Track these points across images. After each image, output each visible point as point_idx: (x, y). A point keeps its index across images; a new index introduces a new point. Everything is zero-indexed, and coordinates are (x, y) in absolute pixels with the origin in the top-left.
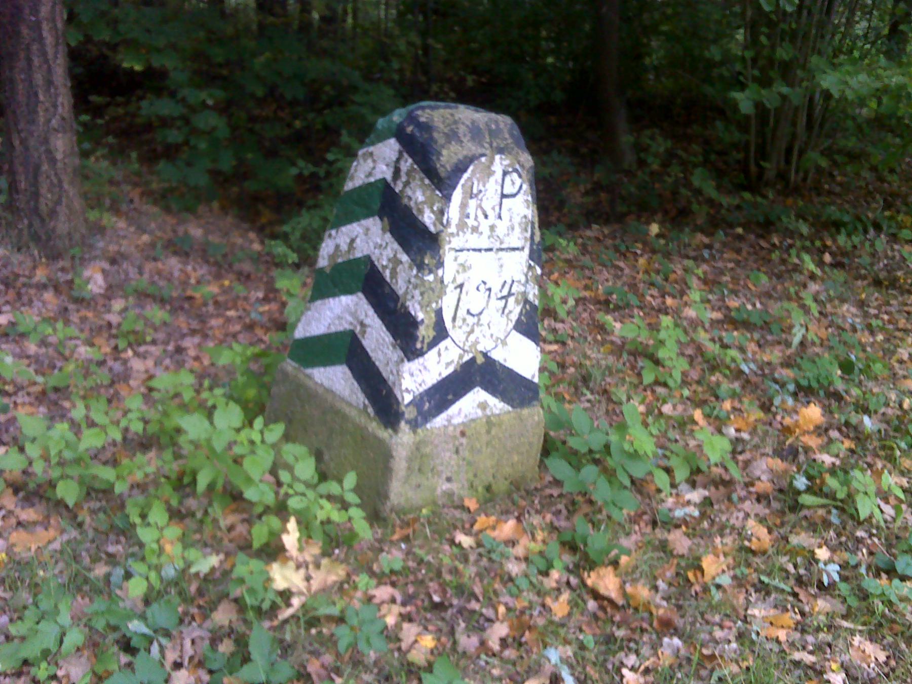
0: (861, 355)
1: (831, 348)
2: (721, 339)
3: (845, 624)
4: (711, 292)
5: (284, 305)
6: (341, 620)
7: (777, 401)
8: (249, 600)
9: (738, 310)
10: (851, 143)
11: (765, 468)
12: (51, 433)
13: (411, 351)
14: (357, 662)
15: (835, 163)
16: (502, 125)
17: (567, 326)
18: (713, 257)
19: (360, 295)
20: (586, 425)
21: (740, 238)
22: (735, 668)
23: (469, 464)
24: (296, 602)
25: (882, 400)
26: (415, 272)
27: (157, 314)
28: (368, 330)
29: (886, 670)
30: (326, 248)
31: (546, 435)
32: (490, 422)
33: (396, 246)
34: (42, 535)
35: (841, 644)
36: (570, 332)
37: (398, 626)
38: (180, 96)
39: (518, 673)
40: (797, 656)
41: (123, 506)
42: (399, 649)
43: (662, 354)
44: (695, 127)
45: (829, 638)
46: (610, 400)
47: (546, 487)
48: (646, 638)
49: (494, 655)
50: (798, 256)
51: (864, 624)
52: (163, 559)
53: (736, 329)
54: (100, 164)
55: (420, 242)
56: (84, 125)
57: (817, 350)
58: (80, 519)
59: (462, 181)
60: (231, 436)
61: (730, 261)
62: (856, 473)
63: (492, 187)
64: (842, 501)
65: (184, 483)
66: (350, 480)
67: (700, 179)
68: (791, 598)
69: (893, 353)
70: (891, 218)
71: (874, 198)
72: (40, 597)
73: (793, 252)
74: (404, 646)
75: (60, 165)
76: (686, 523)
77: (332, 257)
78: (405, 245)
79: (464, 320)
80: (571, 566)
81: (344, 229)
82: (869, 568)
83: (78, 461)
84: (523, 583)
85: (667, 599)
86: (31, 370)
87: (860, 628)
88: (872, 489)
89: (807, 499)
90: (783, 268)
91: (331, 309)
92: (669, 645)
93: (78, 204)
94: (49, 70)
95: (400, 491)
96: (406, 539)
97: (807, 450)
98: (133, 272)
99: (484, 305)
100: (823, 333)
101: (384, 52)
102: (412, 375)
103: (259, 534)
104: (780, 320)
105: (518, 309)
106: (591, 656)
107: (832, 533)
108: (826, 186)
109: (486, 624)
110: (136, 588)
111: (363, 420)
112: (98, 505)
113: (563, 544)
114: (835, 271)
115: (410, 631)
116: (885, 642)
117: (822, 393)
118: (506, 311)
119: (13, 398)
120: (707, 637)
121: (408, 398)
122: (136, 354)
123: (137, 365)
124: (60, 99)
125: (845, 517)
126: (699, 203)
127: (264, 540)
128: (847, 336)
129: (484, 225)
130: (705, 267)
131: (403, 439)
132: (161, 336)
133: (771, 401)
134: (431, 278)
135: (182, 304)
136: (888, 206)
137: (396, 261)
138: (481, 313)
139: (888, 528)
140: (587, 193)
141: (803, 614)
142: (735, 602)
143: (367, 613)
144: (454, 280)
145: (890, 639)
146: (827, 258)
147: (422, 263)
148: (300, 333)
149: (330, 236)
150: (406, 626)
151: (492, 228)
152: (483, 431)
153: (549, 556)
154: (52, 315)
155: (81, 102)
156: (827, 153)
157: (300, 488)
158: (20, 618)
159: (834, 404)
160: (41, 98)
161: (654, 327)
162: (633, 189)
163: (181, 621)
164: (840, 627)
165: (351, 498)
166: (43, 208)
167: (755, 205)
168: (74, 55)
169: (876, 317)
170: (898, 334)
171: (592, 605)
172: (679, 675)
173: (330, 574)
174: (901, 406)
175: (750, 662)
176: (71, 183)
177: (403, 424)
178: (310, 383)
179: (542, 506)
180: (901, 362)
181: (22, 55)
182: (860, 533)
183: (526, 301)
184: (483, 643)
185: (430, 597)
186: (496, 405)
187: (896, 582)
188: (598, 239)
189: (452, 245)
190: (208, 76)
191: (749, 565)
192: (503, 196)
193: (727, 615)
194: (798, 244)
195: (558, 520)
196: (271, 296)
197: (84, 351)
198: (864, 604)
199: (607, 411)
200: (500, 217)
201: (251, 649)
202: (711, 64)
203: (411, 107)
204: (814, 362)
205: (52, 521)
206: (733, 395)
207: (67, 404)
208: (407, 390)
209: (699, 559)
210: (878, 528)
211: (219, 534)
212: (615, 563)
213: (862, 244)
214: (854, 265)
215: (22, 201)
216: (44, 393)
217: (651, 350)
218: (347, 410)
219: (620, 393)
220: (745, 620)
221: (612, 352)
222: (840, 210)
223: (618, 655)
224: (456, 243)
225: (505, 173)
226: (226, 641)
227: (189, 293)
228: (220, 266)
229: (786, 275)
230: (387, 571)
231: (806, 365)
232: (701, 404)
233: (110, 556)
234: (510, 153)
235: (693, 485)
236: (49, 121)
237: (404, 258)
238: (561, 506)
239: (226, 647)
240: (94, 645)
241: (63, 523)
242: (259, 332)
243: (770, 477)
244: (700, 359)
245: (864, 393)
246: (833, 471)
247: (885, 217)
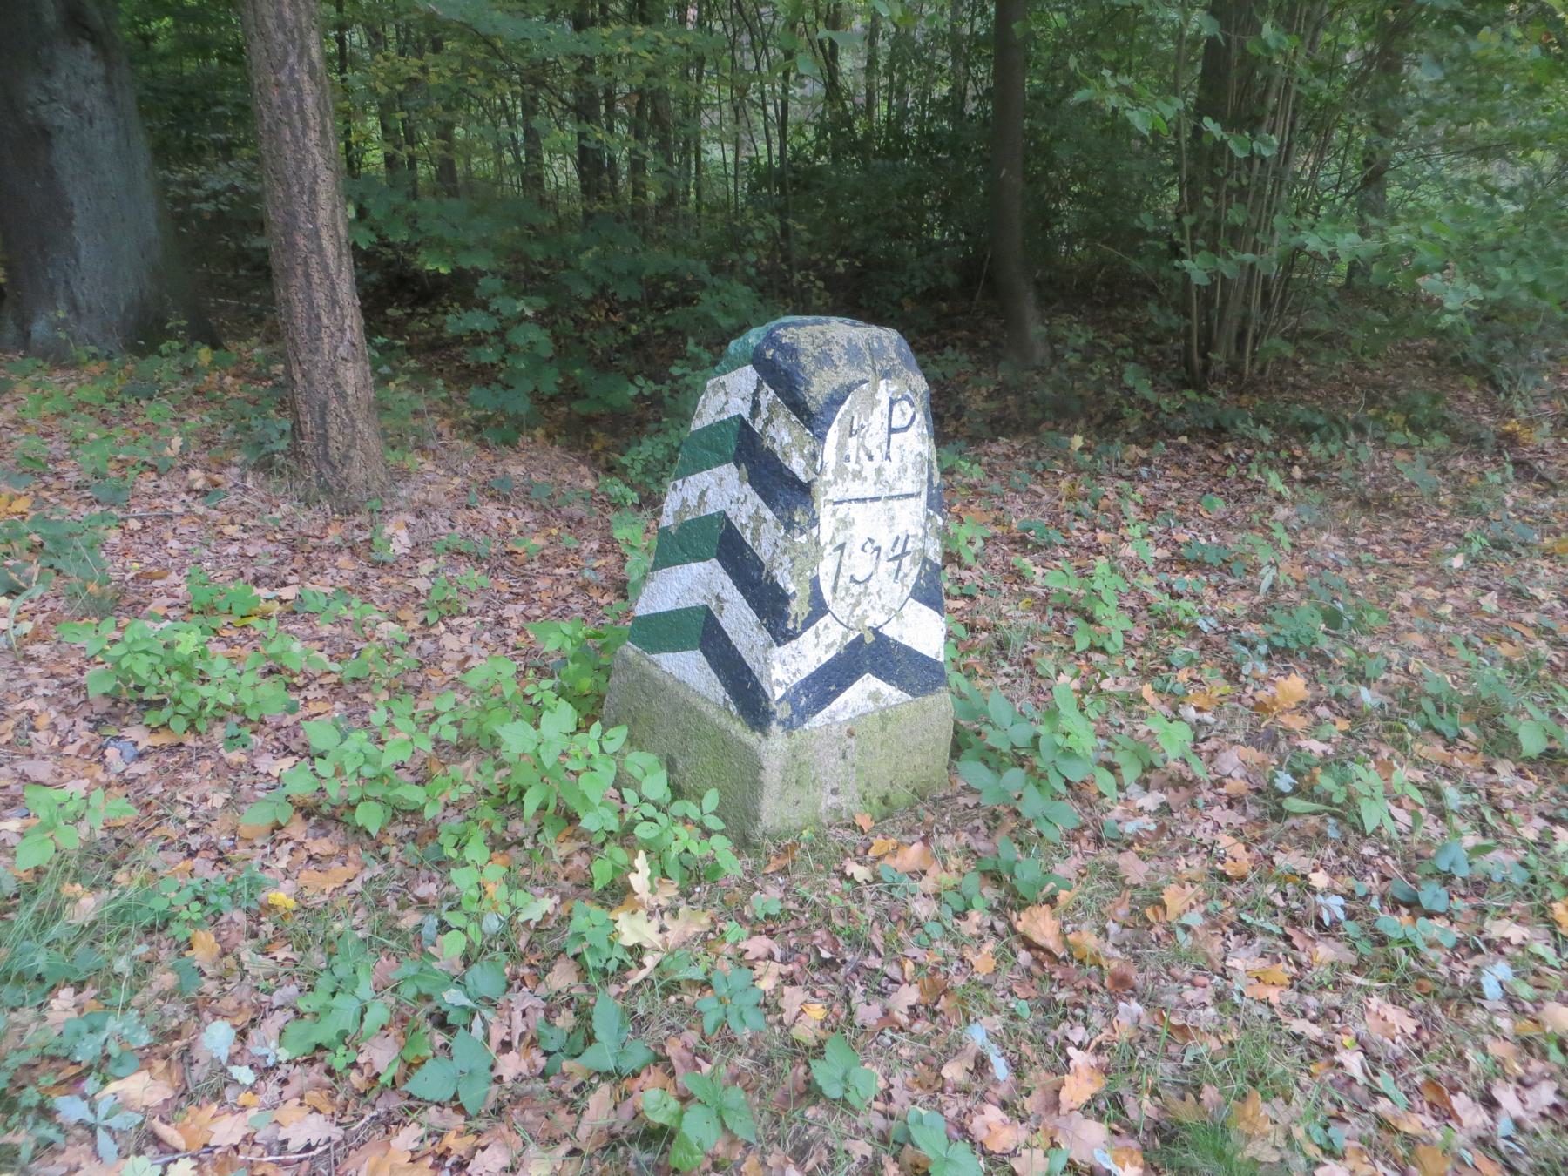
0: (1351, 602)
1: (1309, 594)
2: (1169, 586)
3: (1358, 980)
4: (1152, 522)
5: (623, 558)
6: (706, 985)
7: (1246, 670)
8: (591, 961)
9: (1188, 544)
10: (1324, 325)
11: (1235, 761)
12: (345, 745)
13: (781, 633)
14: (729, 1042)
15: (1300, 350)
16: (886, 343)
17: (975, 575)
18: (1152, 475)
19: (714, 561)
20: (1007, 722)
21: (1185, 449)
22: (1214, 1044)
23: (860, 770)
24: (649, 961)
25: (1383, 663)
26: (782, 532)
27: (472, 576)
28: (726, 605)
29: (1417, 1045)
30: (671, 503)
31: (956, 723)
32: (885, 717)
33: (757, 499)
34: (339, 871)
35: (1352, 1009)
36: (979, 582)
37: (778, 990)
38: (493, 307)
39: (933, 1054)
40: (1299, 1026)
41: (434, 833)
42: (781, 1022)
43: (1099, 611)
44: (1120, 309)
45: (1336, 1000)
46: (1033, 672)
47: (959, 794)
48: (1095, 1002)
49: (901, 1029)
50: (1259, 472)
51: (1382, 980)
52: (485, 904)
53: (1188, 571)
54: (399, 393)
55: (787, 492)
56: (381, 349)
57: (1295, 596)
58: (384, 851)
59: (839, 416)
60: (564, 743)
61: (1174, 479)
62: (1357, 769)
64: (1338, 806)
65: (507, 800)
66: (711, 799)
67: (1131, 375)
68: (1282, 944)
69: (1392, 597)
70: (1377, 418)
71: (1353, 392)
72: (335, 959)
73: (1254, 466)
74: (787, 1019)
75: (351, 401)
76: (1140, 840)
77: (678, 514)
78: (769, 498)
79: (848, 590)
80: (995, 904)
81: (691, 478)
82: (1383, 897)
83: (380, 778)
84: (934, 929)
85: (1120, 946)
86: (324, 656)
87: (1378, 985)
88: (1379, 791)
89: (1293, 804)
90: (1242, 487)
91: (679, 579)
92: (1126, 1012)
93: (375, 446)
94: (333, 288)
95: (774, 811)
96: (784, 871)
97: (1289, 733)
98: (443, 525)
99: (871, 568)
100: (1299, 573)
101: (737, 240)
102: (783, 663)
103: (602, 873)
104: (1240, 557)
105: (915, 571)
106: (1025, 1028)
107: (1330, 851)
108: (1291, 379)
109: (890, 987)
110: (452, 946)
111: (723, 721)
112: (407, 830)
113: (984, 873)
114: (1308, 489)
115: (793, 998)
116: (1412, 1005)
117: (1302, 654)
118: (901, 574)
119: (304, 693)
120: (1176, 999)
121: (779, 692)
122: (450, 629)
123: (450, 642)
124: (348, 321)
125: (1345, 827)
126: (1131, 406)
127: (606, 881)
128: (1329, 576)
129: (869, 468)
130: (1143, 489)
131: (774, 746)
132: (477, 604)
133: (1238, 666)
134: (803, 539)
135: (505, 561)
136: (1372, 401)
137: (758, 519)
138: (868, 579)
139: (1404, 842)
140: (990, 397)
141: (1299, 965)
142: (1209, 950)
143: (739, 978)
144: (833, 538)
145: (1418, 1001)
146: (1297, 472)
147: (791, 519)
148: (641, 610)
149: (675, 487)
150: (787, 990)
151: (879, 471)
152: (877, 728)
153: (967, 892)
154: (348, 583)
156: (1292, 337)
157: (650, 810)
158: (311, 988)
159: (1320, 672)
160: (325, 321)
161: (1083, 573)
162: (1048, 391)
163: (510, 986)
164: (1351, 984)
165: (713, 823)
166: (335, 455)
167: (1202, 408)
168: (363, 259)
169: (1366, 549)
170: (1396, 571)
171: (1024, 957)
172: (1141, 1054)
173: (691, 923)
174: (1406, 670)
175: (1235, 1035)
176: (365, 421)
177: (774, 724)
178: (657, 673)
179: (956, 823)
180: (1403, 610)
181: (299, 271)
182: (1367, 851)
183: (925, 561)
184: (886, 1012)
185: (818, 952)
186: (891, 694)
187: (1422, 921)
188: (1008, 457)
189: (829, 497)
190: (524, 280)
191: (1224, 897)
192: (892, 431)
193: (1199, 968)
194: (1259, 455)
195: (976, 840)
196: (608, 547)
197: (389, 629)
198: (1380, 950)
199: (1031, 690)
200: (888, 457)
201: (595, 1026)
202: (1141, 233)
203: (771, 324)
204: (1290, 614)
205: (351, 854)
206: (1191, 661)
207: (367, 697)
208: (779, 683)
209: (1158, 889)
210: (1390, 842)
211: (552, 869)
212: (1051, 901)
213: (1342, 452)
214: (1333, 481)
215: (307, 446)
216: (340, 684)
217: (1083, 603)
218: (704, 707)
219: (1047, 664)
220: (1223, 976)
221: (1033, 608)
222: (1311, 410)
223: (1061, 1028)
224: (834, 493)
225: (892, 402)
226: (564, 1011)
227: (510, 547)
228: (548, 510)
229: (1246, 497)
230: (762, 917)
231: (1280, 617)
232: (1149, 675)
233: (422, 901)
234: (898, 377)
235: (1146, 785)
236: (337, 348)
237: (768, 514)
238: (978, 822)
239: (565, 1020)
240: (402, 1021)
241: (365, 856)
242: (595, 594)
243: (1244, 772)
244: (1144, 613)
245: (1358, 654)
246: (1325, 763)
247: (1370, 418)
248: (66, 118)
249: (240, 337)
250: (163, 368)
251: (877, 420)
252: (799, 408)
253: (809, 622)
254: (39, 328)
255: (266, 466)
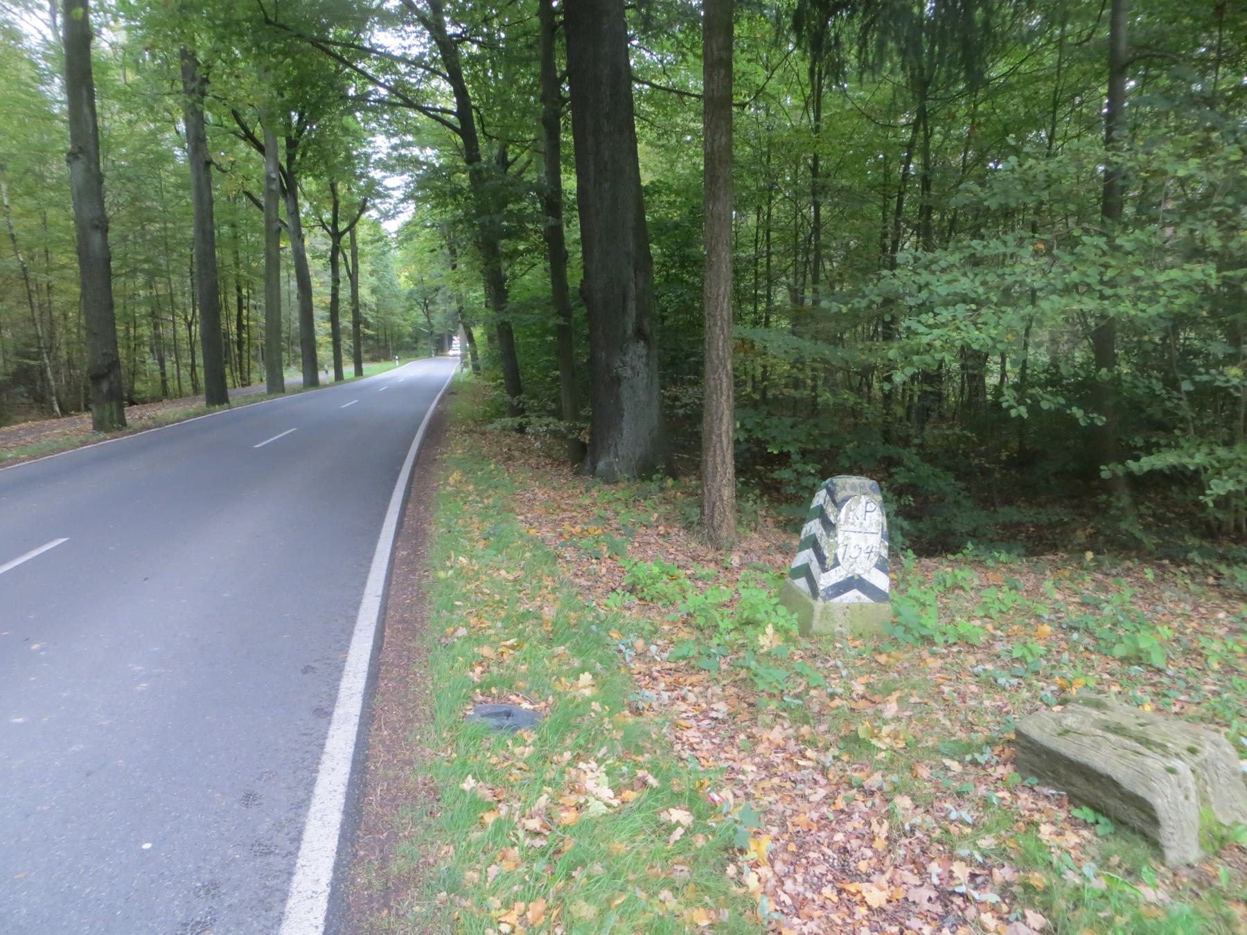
13: (825, 570)
32: (862, 606)
55: (829, 526)
63: (861, 508)
93: (732, 522)
98: (755, 559)
121: (821, 588)
129: (857, 522)
131: (819, 604)
155: (739, 472)
166: (715, 524)
186: (865, 599)
248: (628, 373)
249: (686, 475)
250: (653, 486)
251: (861, 508)
252: (834, 501)
253: (833, 567)
254: (601, 465)
255: (688, 527)
